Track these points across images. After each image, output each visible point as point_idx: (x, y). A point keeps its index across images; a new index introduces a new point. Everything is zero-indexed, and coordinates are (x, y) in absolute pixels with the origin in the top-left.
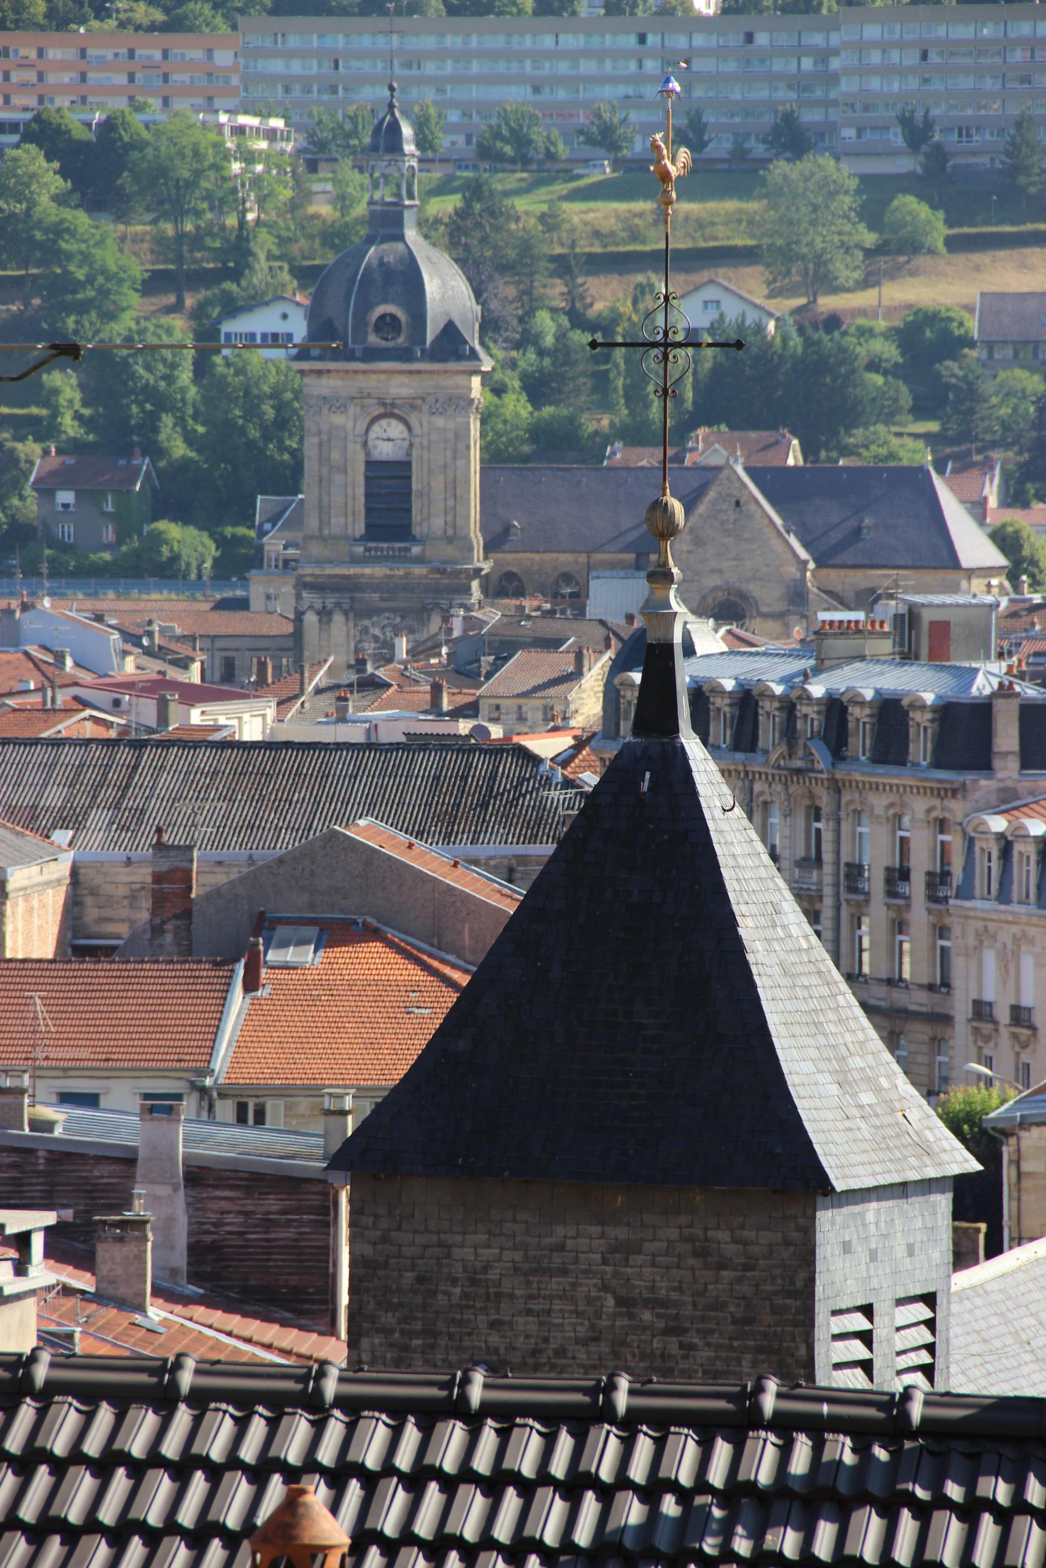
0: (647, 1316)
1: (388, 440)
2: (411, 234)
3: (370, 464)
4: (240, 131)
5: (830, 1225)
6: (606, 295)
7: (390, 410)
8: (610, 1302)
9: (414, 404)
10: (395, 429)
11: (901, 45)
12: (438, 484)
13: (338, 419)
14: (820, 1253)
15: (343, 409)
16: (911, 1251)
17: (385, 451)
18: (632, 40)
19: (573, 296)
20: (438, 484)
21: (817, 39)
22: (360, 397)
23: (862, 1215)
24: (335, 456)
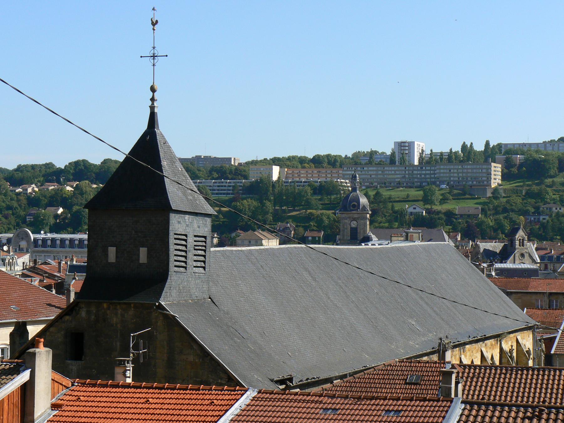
0: (140, 234)
1: (354, 224)
2: (358, 192)
3: (351, 228)
4: (341, 182)
5: (174, 218)
6: (397, 207)
7: (354, 219)
8: (133, 232)
9: (358, 218)
10: (355, 222)
11: (446, 169)
12: (362, 231)
13: (346, 221)
14: (171, 222)
15: (347, 219)
16: (199, 227)
17: (353, 226)
18: (404, 168)
19: (393, 206)
20: (362, 231)
21: (433, 168)
22: (349, 218)
23: (184, 217)
24: (345, 227)
